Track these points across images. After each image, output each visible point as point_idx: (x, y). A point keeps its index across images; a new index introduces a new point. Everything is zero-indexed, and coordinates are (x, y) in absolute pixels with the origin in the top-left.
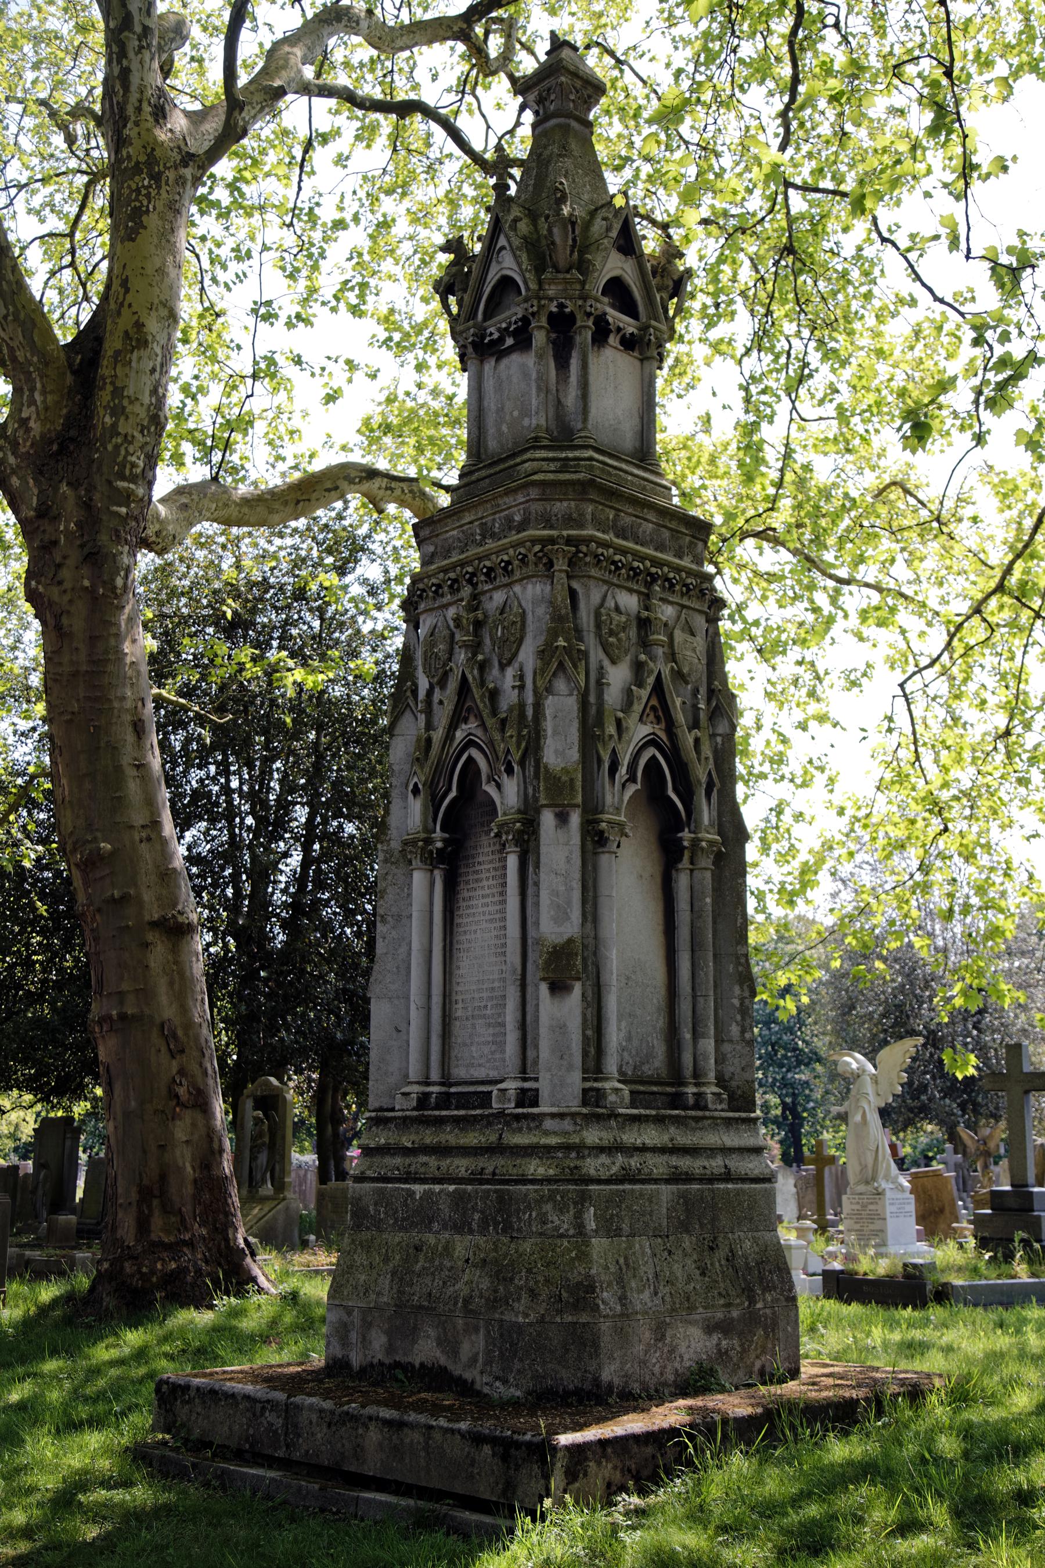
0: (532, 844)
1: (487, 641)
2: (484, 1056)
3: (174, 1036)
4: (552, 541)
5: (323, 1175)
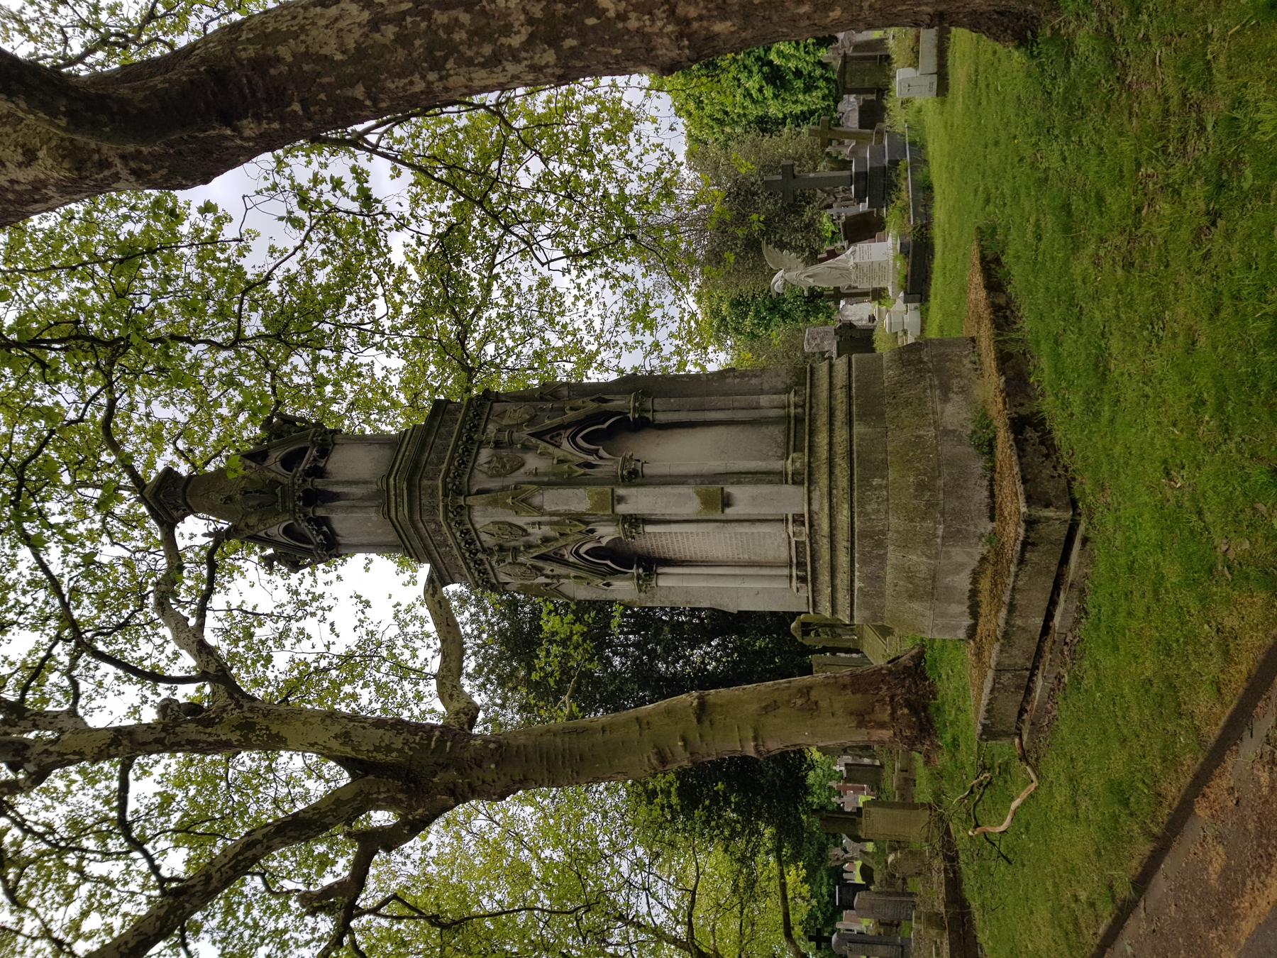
1: (513, 543)
2: (775, 543)
3: (765, 708)
4: (446, 506)
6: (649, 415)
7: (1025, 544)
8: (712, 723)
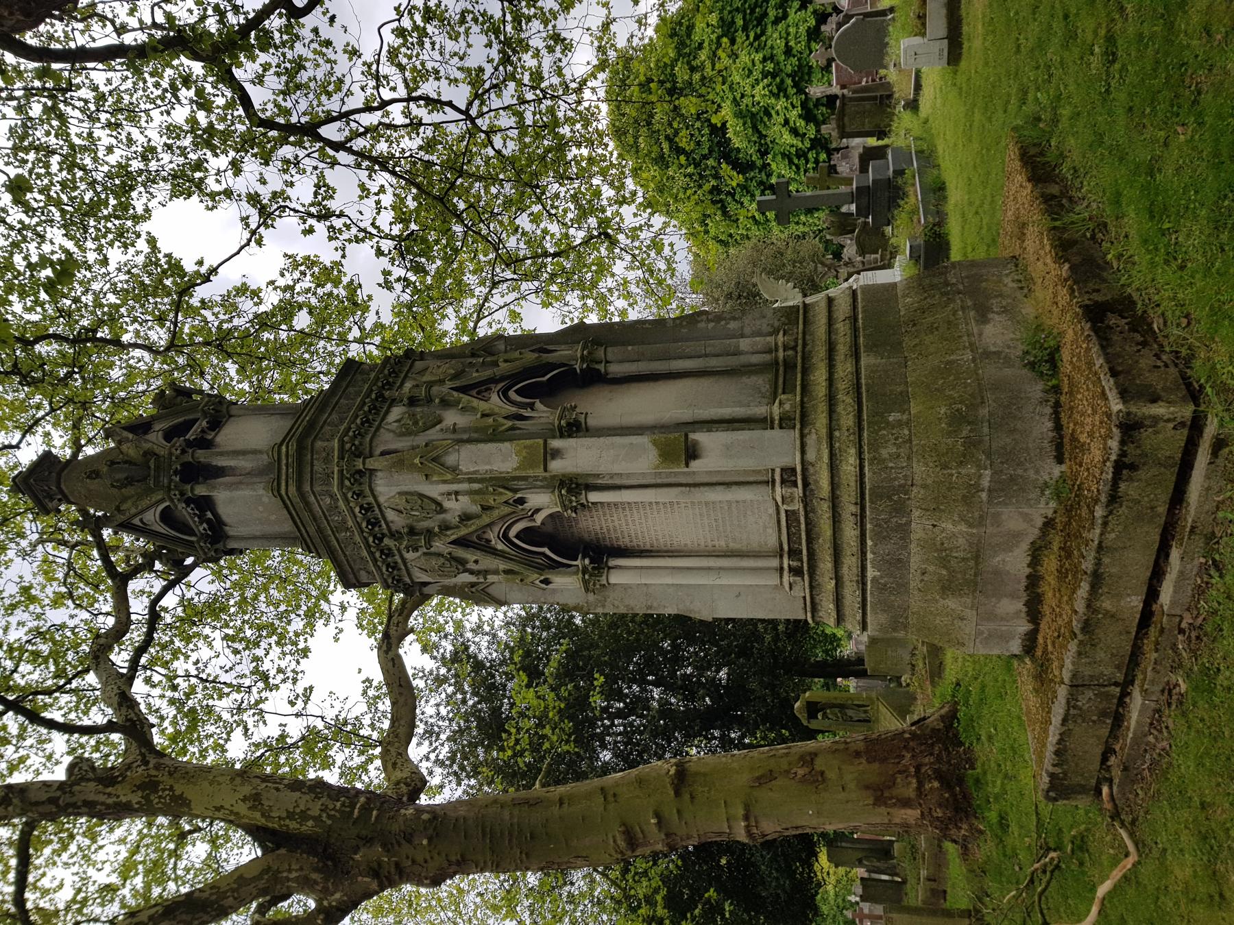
0: (580, 481)
2: (757, 518)
3: (758, 778)
4: (341, 472)
5: (861, 674)
6: (601, 367)
7: (1119, 467)
8: (692, 798)
